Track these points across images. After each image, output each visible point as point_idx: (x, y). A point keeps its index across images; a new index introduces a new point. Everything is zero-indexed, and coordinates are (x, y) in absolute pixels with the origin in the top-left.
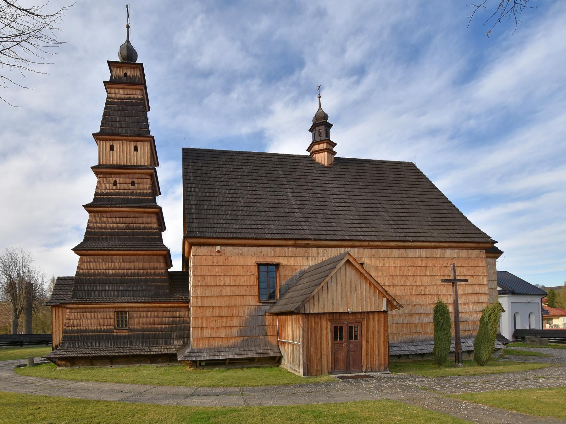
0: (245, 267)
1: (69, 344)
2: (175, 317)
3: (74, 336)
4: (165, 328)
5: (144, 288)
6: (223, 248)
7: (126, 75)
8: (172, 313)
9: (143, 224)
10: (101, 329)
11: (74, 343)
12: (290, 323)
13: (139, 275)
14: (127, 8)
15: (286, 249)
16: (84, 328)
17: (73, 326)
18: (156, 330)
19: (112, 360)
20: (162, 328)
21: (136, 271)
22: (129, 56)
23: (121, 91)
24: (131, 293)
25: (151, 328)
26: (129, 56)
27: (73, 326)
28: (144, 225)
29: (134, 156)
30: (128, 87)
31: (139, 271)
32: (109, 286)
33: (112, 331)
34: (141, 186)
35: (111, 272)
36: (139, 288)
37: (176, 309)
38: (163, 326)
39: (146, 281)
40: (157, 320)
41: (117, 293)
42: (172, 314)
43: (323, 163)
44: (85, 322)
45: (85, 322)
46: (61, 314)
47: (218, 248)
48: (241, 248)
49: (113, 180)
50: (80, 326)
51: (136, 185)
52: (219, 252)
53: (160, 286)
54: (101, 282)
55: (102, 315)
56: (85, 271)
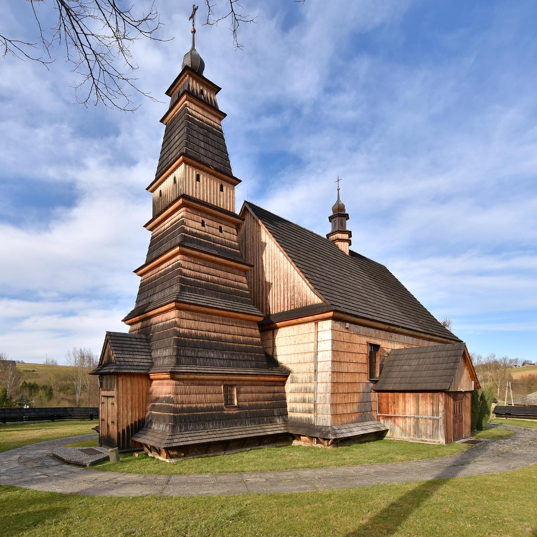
0: (335, 342)
1: (181, 428)
2: (274, 392)
3: (185, 416)
4: (268, 404)
5: (246, 357)
6: (353, 326)
7: (202, 92)
8: (272, 387)
9: (236, 281)
10: (211, 406)
11: (185, 426)
12: (136, 383)
13: (239, 342)
14: (195, 10)
15: (381, 331)
16: (194, 406)
17: (182, 403)
18: (261, 407)
19: (226, 446)
20: (265, 404)
21: (193, 331)
22: (194, 69)
23: (200, 111)
24: (235, 362)
25: (257, 405)
26: (194, 69)
27: (182, 403)
28: (236, 283)
29: (220, 196)
30: (209, 109)
31: (239, 337)
32: (213, 352)
33: (221, 409)
34: (227, 235)
35: (213, 335)
36: (241, 357)
37: (274, 383)
38: (266, 402)
39: (247, 350)
40: (261, 396)
41: (222, 362)
42: (272, 389)
43: (228, 210)
44: (193, 398)
45: (193, 398)
46: (129, 385)
47: (348, 325)
48: (359, 326)
49: (219, 225)
50: (190, 403)
51: (206, 227)
52: (347, 328)
53: (259, 356)
54: (195, 346)
55: (210, 389)
56: (186, 331)
